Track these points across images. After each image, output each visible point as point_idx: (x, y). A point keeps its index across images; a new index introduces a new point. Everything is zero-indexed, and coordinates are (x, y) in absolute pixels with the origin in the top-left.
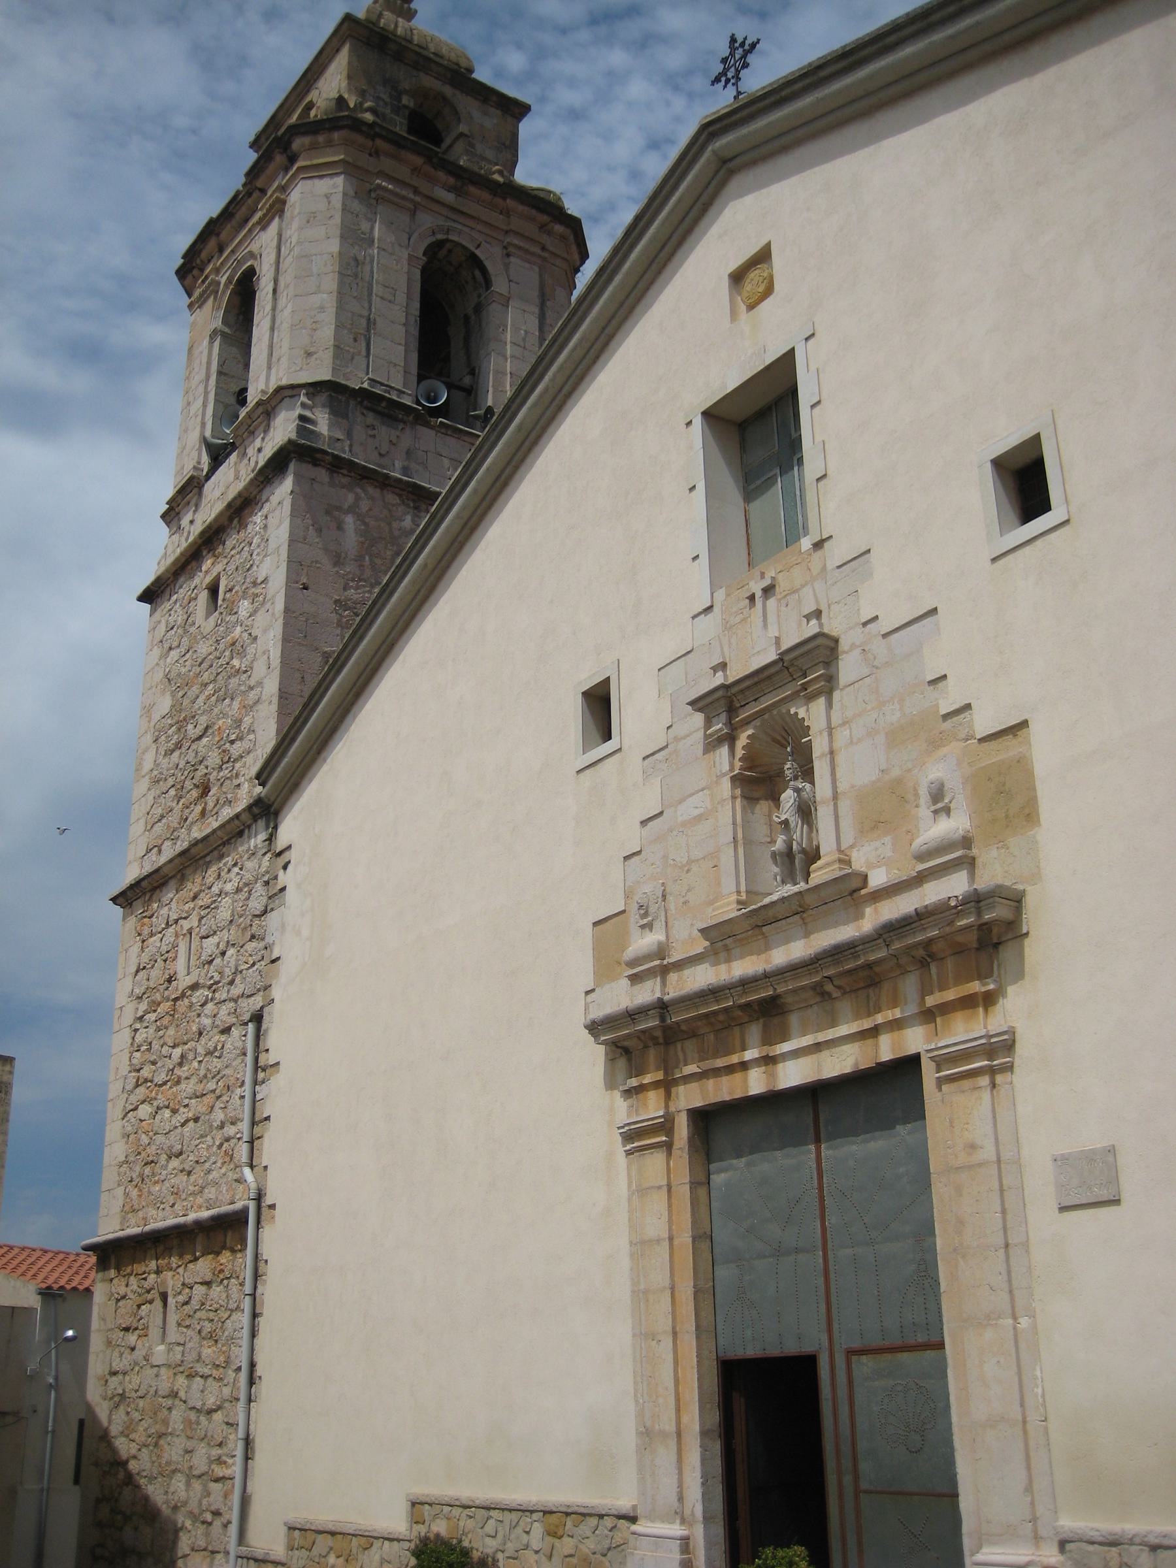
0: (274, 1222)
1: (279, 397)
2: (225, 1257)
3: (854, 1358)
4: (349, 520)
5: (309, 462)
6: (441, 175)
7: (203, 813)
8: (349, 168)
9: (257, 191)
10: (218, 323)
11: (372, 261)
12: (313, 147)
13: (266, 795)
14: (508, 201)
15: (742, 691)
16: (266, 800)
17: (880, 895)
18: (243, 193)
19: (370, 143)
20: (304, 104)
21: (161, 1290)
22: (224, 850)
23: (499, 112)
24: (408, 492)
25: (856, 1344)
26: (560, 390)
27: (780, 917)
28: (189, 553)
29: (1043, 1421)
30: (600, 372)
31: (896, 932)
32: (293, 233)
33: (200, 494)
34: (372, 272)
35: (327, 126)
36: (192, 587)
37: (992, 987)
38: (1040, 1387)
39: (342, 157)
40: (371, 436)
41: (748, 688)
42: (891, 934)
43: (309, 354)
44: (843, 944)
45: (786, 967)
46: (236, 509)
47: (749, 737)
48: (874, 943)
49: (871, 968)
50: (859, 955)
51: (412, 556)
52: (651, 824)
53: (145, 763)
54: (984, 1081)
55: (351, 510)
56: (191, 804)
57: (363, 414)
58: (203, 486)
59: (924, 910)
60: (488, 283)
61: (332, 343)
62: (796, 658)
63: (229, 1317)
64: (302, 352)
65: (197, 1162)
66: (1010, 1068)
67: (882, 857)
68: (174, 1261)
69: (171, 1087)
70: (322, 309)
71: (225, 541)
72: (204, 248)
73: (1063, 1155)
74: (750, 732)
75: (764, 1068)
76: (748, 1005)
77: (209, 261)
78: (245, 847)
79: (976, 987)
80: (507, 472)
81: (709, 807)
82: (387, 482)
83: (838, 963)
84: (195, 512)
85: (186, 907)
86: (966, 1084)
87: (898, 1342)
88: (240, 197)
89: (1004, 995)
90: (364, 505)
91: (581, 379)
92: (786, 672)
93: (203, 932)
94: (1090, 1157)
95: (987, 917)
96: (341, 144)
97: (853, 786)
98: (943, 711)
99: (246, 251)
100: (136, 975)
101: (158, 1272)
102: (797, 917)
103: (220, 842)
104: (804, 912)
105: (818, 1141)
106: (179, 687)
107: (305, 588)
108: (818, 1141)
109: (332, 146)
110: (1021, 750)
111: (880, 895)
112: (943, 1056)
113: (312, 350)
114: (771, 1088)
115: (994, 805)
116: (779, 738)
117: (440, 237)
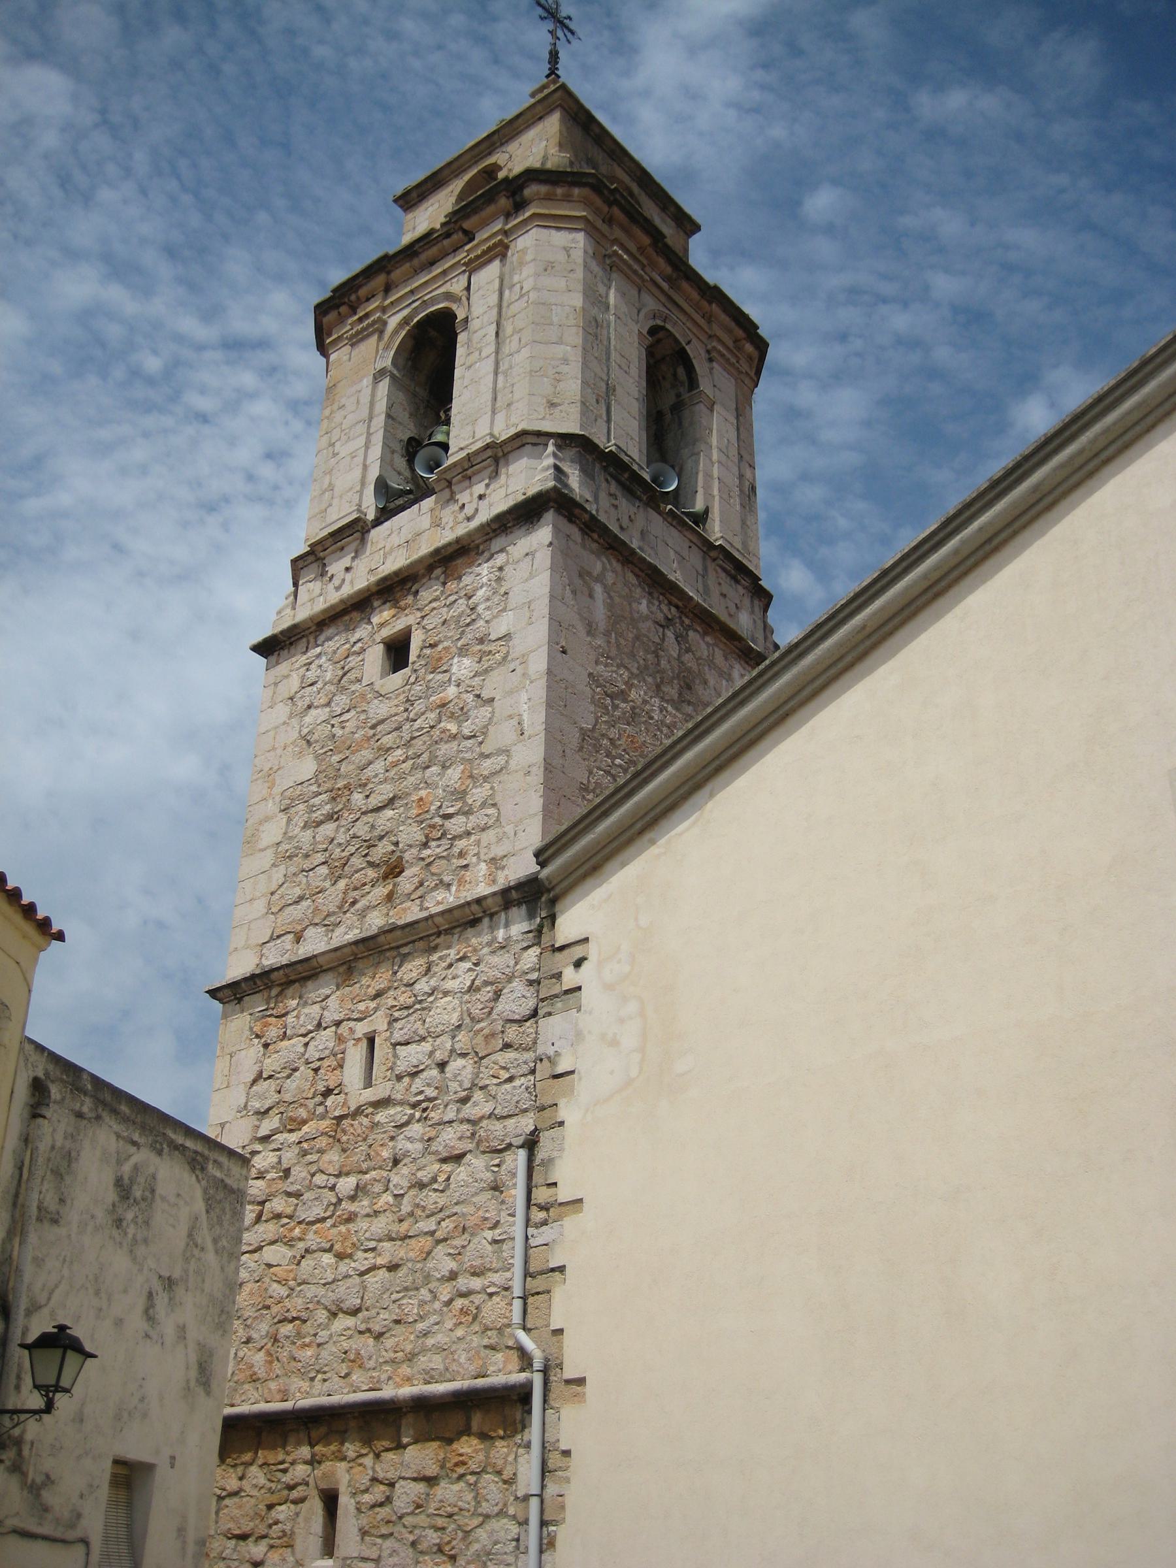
0: (585, 1401)
1: (518, 443)
2: (501, 1449)
4: (598, 589)
5: (565, 517)
6: (661, 262)
7: (390, 897)
8: (591, 229)
9: (460, 234)
10: (387, 361)
11: (609, 326)
12: (549, 198)
13: (547, 878)
14: (714, 305)
16: (546, 883)
18: (439, 233)
19: (605, 209)
20: (483, 165)
21: (323, 1486)
22: (438, 941)
23: (673, 224)
24: (646, 574)
26: (1096, 455)
28: (353, 601)
30: (1161, 441)
32: (525, 277)
33: (363, 541)
34: (609, 339)
35: (569, 179)
36: (353, 640)
39: (584, 214)
40: (613, 505)
43: (552, 405)
46: (445, 557)
51: (842, 615)
53: (263, 835)
55: (600, 579)
56: (364, 884)
57: (607, 480)
58: (368, 531)
60: (693, 383)
61: (578, 397)
63: (481, 1524)
64: (545, 401)
65: (397, 1322)
68: (350, 1449)
69: (334, 1226)
70: (565, 361)
71: (417, 592)
72: (365, 284)
77: (368, 300)
78: (486, 938)
80: (1003, 535)
82: (630, 559)
84: (353, 559)
85: (362, 1006)
88: (436, 235)
90: (610, 578)
91: (1127, 446)
93: (398, 1036)
96: (581, 202)
99: (433, 294)
100: (252, 1085)
101: (313, 1462)
103: (436, 930)
106: (331, 750)
107: (564, 652)
109: (569, 201)
113: (555, 401)
117: (659, 322)
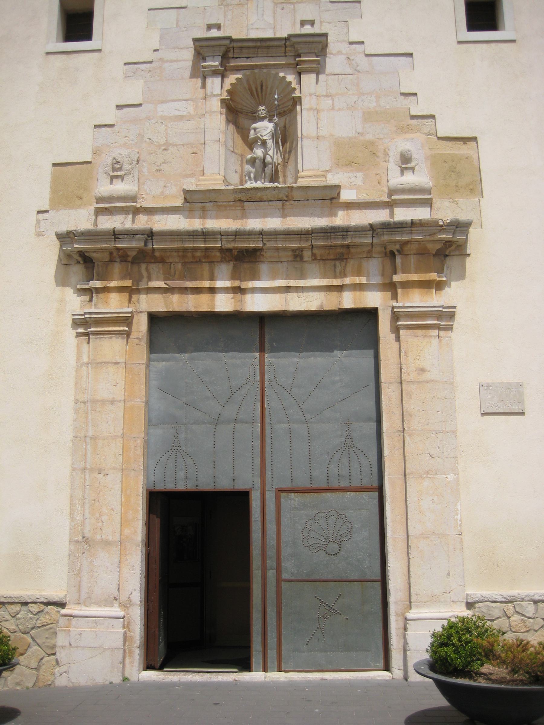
3: (283, 495)
15: (241, 48)
17: (350, 206)
25: (287, 485)
27: (265, 199)
29: (460, 535)
31: (389, 230)
37: (444, 279)
38: (459, 515)
41: (249, 47)
42: (385, 230)
44: (386, 222)
45: (284, 231)
47: (237, 79)
48: (364, 233)
49: (349, 248)
50: (347, 238)
52: (126, 110)
54: (434, 332)
59: (418, 222)
62: (299, 43)
66: (449, 328)
67: (354, 184)
73: (488, 384)
74: (240, 76)
75: (232, 295)
76: (230, 250)
79: (434, 276)
81: (192, 112)
83: (328, 239)
86: (420, 332)
87: (324, 485)
89: (449, 286)
92: (284, 49)
94: (508, 387)
95: (458, 237)
97: (332, 135)
98: (413, 113)
102: (281, 203)
104: (286, 201)
105: (262, 350)
108: (262, 350)
110: (469, 152)
111: (350, 206)
112: (406, 313)
114: (239, 309)
115: (448, 177)
116: (254, 88)
